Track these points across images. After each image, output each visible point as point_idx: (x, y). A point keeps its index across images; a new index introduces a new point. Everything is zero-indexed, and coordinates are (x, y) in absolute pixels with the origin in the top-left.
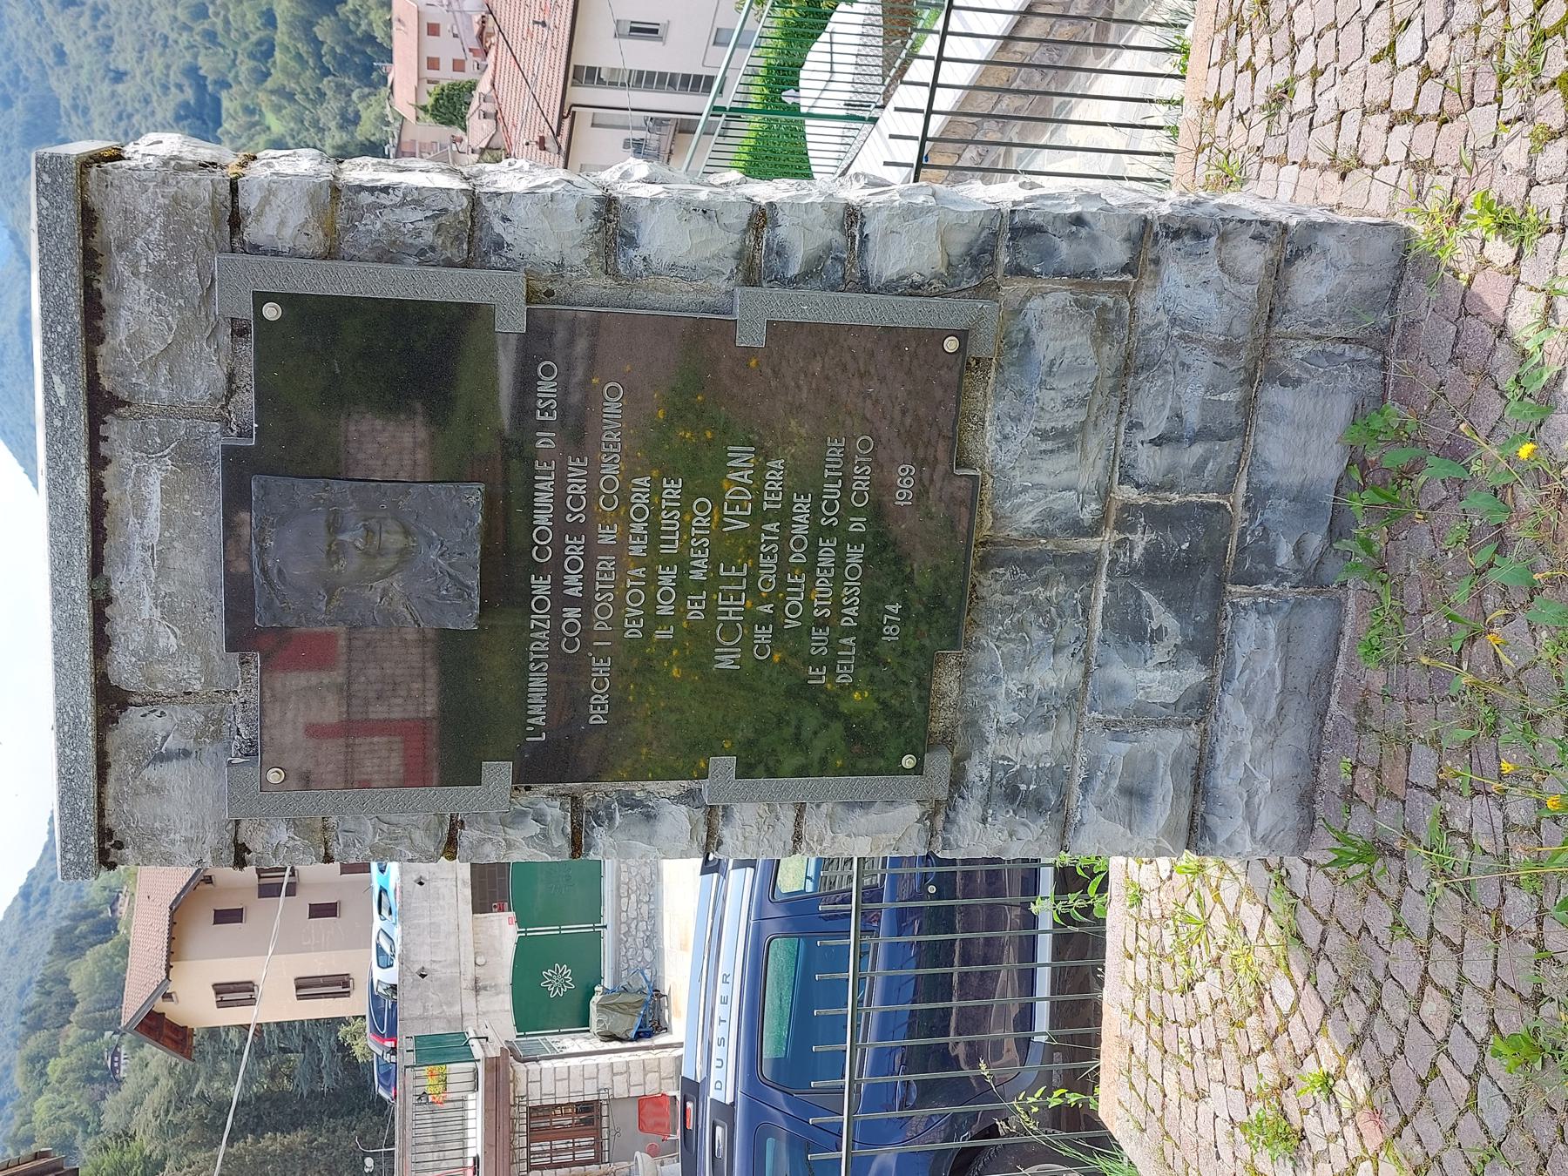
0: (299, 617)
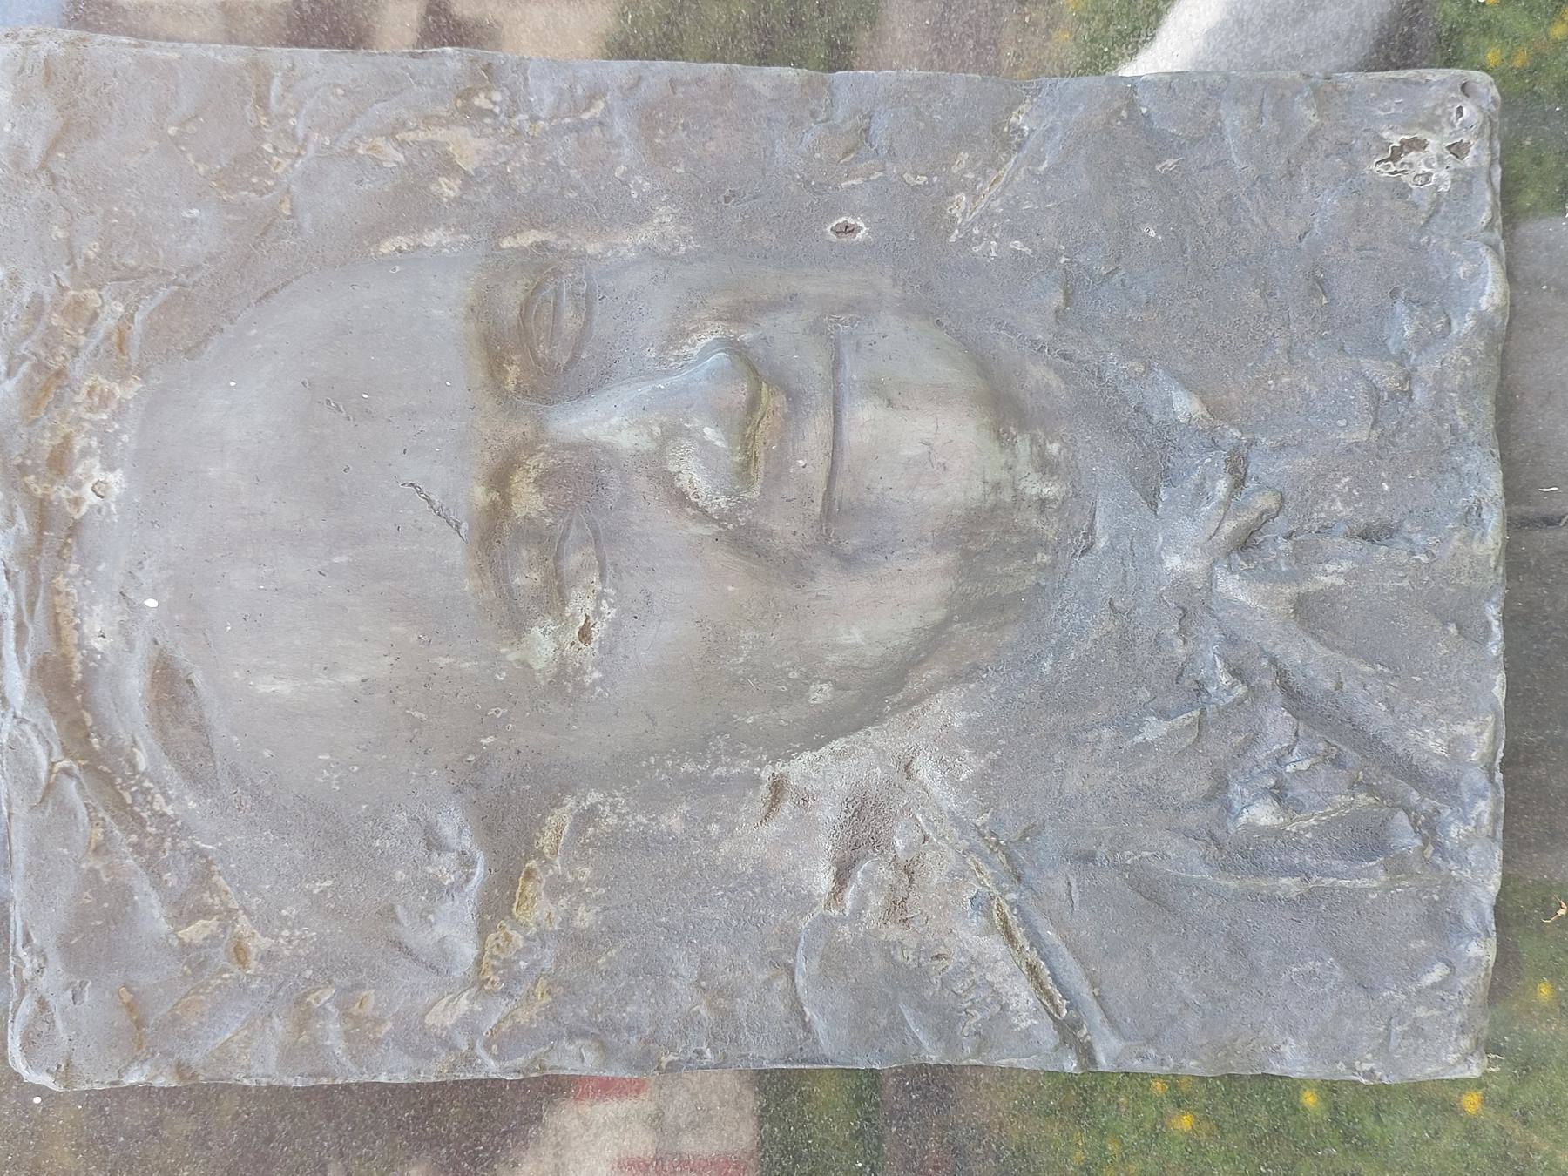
0: (304, 1017)
